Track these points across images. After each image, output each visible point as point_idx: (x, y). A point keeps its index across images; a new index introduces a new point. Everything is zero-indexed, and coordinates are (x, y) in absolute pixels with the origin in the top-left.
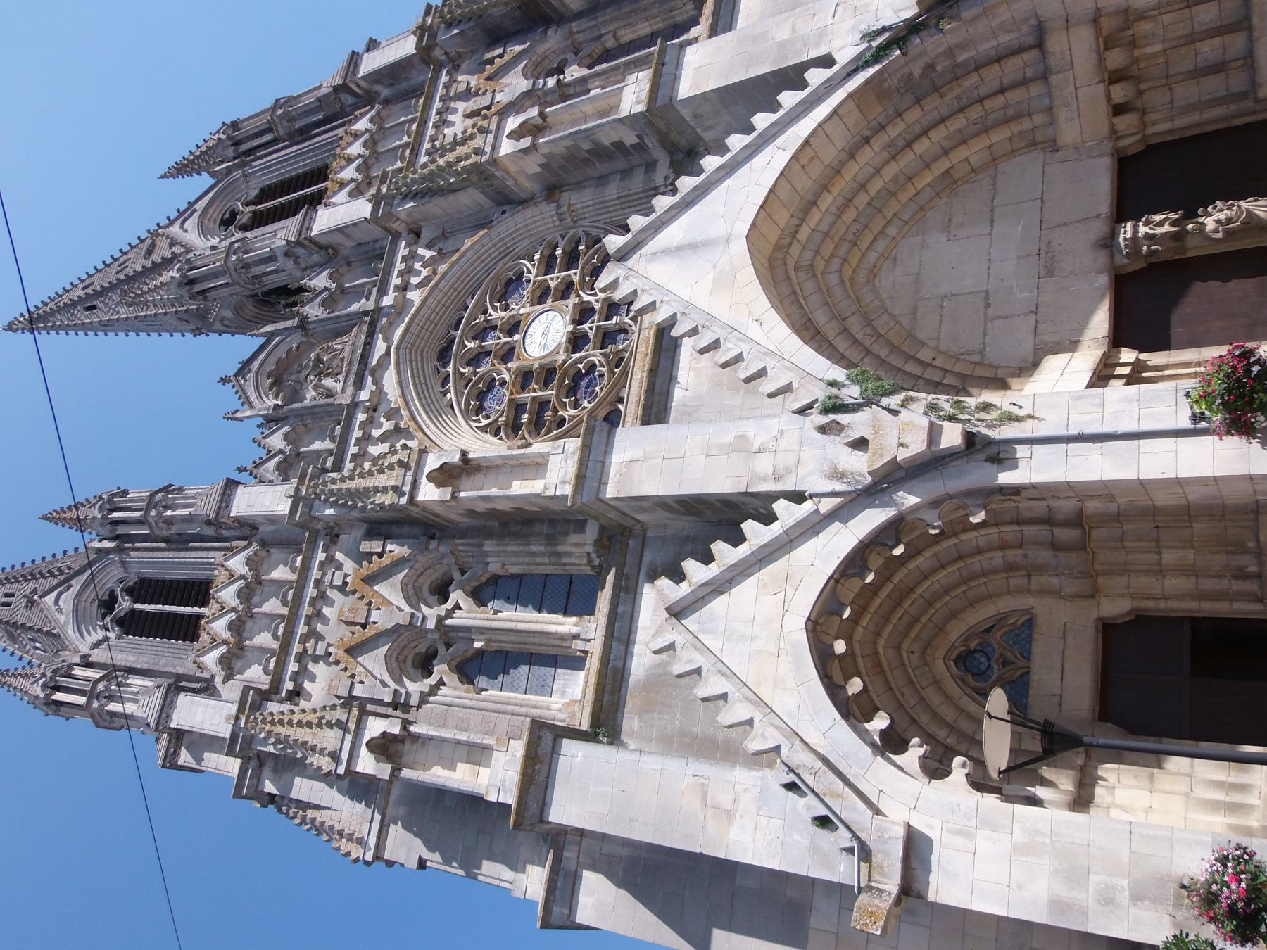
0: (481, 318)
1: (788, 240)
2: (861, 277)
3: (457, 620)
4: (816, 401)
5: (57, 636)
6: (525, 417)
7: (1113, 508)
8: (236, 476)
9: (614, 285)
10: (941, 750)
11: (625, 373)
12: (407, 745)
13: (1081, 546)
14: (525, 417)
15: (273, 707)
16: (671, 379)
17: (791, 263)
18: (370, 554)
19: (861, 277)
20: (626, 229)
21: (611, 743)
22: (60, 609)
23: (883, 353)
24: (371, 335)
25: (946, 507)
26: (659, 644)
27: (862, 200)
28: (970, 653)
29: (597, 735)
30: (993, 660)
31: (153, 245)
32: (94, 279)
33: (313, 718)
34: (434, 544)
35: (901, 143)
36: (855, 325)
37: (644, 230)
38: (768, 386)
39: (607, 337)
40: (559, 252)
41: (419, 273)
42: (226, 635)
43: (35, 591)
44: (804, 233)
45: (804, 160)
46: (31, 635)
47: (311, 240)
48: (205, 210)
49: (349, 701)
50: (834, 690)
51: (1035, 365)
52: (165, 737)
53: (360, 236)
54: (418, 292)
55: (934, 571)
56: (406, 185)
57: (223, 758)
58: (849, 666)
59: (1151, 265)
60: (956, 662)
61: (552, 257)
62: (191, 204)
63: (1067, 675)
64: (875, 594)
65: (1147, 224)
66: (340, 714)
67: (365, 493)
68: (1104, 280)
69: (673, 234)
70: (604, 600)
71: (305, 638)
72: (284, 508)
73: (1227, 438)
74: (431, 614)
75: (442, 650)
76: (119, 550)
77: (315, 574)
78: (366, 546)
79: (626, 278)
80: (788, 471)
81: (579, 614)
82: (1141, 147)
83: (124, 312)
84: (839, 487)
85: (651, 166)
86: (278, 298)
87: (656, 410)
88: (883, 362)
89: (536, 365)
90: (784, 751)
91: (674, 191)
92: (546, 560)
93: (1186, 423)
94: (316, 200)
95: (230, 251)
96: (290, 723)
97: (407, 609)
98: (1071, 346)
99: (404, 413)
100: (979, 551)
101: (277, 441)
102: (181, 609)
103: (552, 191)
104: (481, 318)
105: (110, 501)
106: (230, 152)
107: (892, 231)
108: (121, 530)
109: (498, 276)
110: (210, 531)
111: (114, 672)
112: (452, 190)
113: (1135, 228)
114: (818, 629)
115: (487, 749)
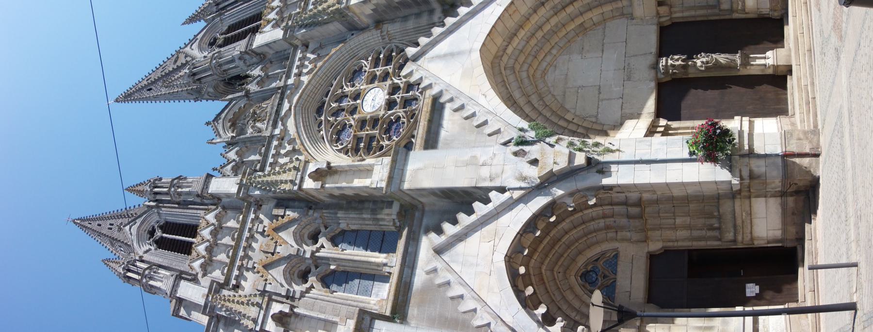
0: (340, 91)
1: (501, 53)
2: (538, 74)
3: (322, 254)
4: (512, 139)
5: (129, 246)
6: (362, 145)
7: (655, 197)
8: (211, 173)
9: (410, 74)
10: (572, 323)
11: (416, 122)
12: (293, 319)
13: (640, 216)
14: (362, 145)
15: (225, 292)
16: (439, 125)
17: (502, 65)
18: (278, 216)
19: (538, 74)
20: (417, 44)
21: (401, 323)
22: (131, 232)
23: (548, 115)
24: (282, 99)
25: (577, 196)
26: (430, 267)
27: (540, 34)
28: (588, 272)
29: (394, 318)
30: (599, 275)
31: (178, 57)
32: (152, 76)
33: (245, 300)
34: (311, 212)
35: (560, 7)
36: (534, 99)
37: (427, 45)
38: (488, 130)
39: (407, 102)
40: (381, 56)
41: (307, 67)
42: (204, 253)
43: (121, 224)
44: (510, 50)
45: (511, 12)
46: (120, 244)
47: (252, 51)
48: (202, 39)
49: (263, 293)
50: (519, 293)
51: (622, 124)
52: (174, 301)
53: (278, 48)
54: (307, 77)
55: (571, 230)
56: (301, 21)
57: (200, 315)
58: (527, 280)
59: (674, 80)
60: (581, 277)
61: (378, 59)
62: (195, 36)
63: (632, 282)
64: (541, 242)
65: (672, 59)
66: (258, 300)
67: (275, 183)
68: (653, 84)
69: (442, 47)
70: (401, 245)
71: (242, 259)
72: (234, 189)
73: (705, 163)
74: (308, 250)
75: (313, 269)
76: (157, 207)
77: (249, 225)
78: (276, 212)
79: (417, 70)
80: (498, 176)
81: (387, 252)
82: (669, 23)
83: (164, 91)
84: (523, 185)
85: (431, 12)
86: (235, 81)
87: (431, 143)
88: (547, 120)
89: (368, 117)
90: (492, 326)
91: (444, 25)
92: (371, 222)
93: (687, 156)
94: (255, 30)
95: (212, 58)
96: (233, 301)
97: (296, 246)
98: (637, 116)
99: (298, 141)
100: (593, 219)
101: (232, 155)
102: (184, 238)
103: (378, 23)
104: (340, 91)
105: (154, 183)
106: (215, 9)
107: (554, 52)
108: (158, 197)
109: (349, 69)
110: (198, 200)
111: (152, 266)
112: (325, 23)
113: (667, 60)
114: (511, 261)
115: (335, 324)
